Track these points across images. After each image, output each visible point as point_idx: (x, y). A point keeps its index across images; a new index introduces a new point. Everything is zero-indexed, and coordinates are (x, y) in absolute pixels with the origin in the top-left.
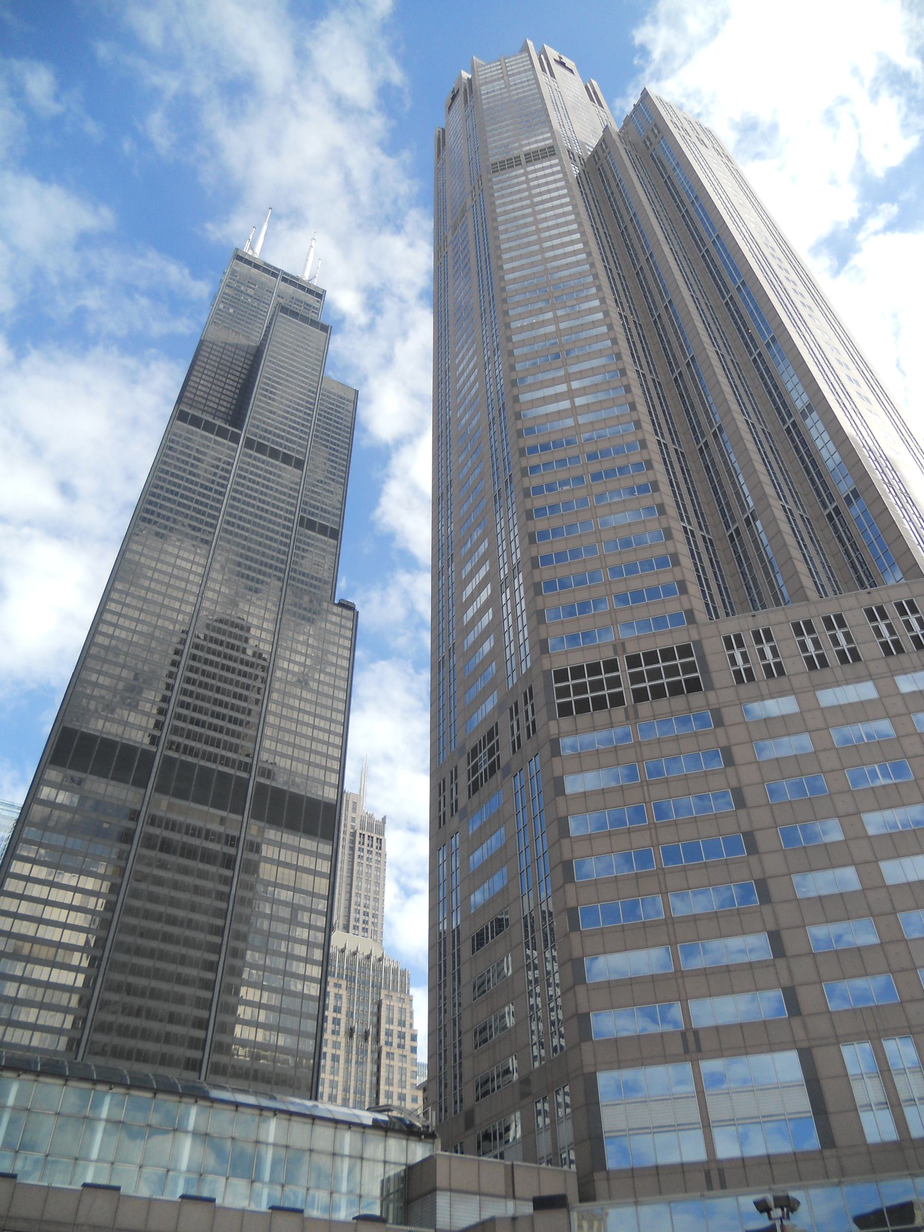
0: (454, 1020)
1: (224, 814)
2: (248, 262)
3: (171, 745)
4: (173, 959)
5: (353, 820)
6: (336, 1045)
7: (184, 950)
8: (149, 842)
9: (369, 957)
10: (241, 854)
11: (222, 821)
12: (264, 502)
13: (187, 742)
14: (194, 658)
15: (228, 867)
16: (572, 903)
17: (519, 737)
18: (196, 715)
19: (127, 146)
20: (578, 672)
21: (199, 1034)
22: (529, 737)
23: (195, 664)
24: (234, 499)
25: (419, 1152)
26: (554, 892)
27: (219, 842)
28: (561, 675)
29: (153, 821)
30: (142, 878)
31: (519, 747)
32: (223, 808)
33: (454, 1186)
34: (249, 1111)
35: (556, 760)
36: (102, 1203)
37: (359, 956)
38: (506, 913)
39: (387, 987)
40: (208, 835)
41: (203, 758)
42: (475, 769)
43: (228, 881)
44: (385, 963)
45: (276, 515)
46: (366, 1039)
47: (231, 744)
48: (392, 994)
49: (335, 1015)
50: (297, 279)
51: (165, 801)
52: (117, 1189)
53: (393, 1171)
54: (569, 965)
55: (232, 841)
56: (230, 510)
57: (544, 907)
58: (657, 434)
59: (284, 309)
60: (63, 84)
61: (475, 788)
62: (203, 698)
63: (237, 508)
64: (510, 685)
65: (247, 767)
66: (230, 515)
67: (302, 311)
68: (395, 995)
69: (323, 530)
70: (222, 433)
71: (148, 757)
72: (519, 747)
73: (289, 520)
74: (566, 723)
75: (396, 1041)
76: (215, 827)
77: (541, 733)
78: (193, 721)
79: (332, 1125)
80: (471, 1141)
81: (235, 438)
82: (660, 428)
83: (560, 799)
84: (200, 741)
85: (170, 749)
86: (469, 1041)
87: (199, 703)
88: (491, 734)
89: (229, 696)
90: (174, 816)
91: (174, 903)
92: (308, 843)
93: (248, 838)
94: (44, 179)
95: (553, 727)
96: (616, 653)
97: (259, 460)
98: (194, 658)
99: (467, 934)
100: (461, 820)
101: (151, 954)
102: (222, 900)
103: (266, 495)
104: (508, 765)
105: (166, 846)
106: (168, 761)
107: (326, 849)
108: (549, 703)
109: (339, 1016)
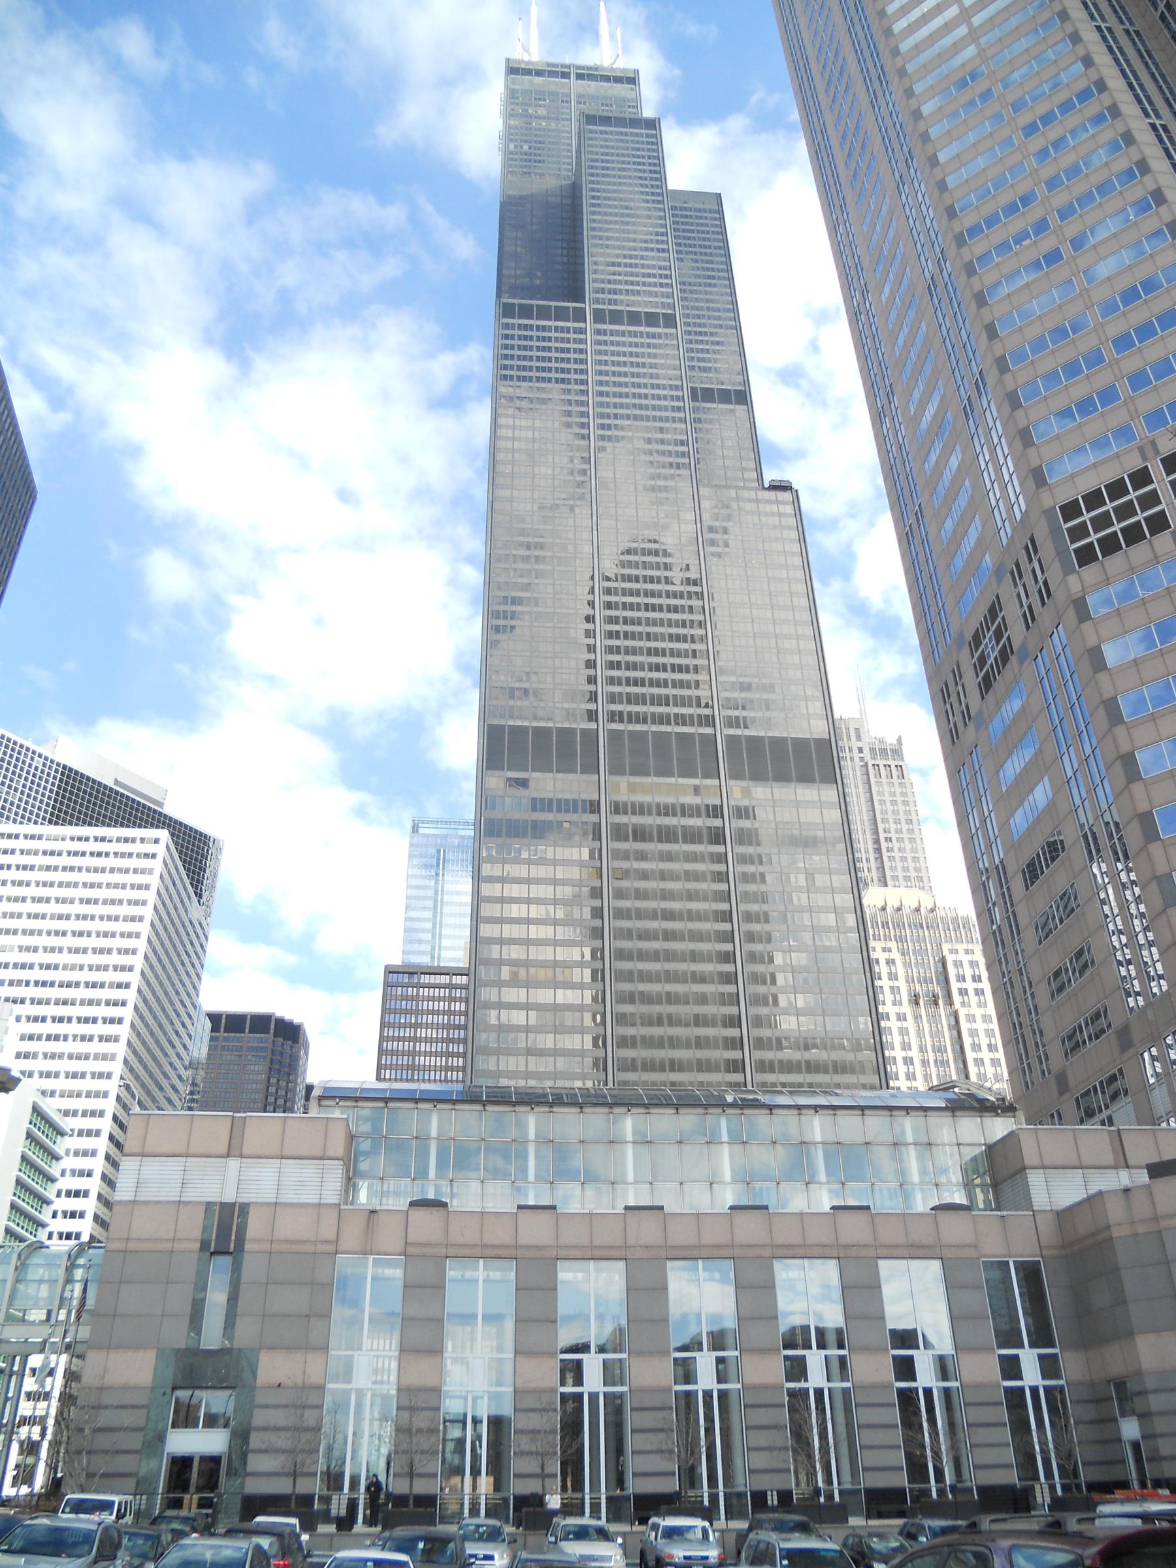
0: (1020, 970)
1: (696, 781)
2: (528, 72)
3: (613, 717)
4: (682, 957)
5: (861, 750)
6: (901, 1017)
7: (692, 946)
8: (619, 833)
9: (918, 910)
10: (731, 825)
11: (696, 790)
12: (639, 386)
13: (630, 708)
14: (609, 606)
15: (718, 843)
16: (1143, 806)
17: (1030, 608)
18: (632, 674)
19: (253, 79)
20: (1094, 499)
21: (733, 1032)
22: (1043, 603)
23: (613, 613)
24: (601, 394)
25: (999, 1127)
26: (1116, 797)
27: (699, 816)
28: (1070, 510)
29: (617, 808)
30: (625, 874)
31: (1033, 619)
32: (693, 775)
33: (1046, 1163)
34: (785, 1112)
35: (1087, 626)
36: (649, 1222)
37: (906, 911)
38: (1059, 833)
40: (686, 811)
41: (653, 723)
42: (982, 660)
43: (722, 858)
44: (940, 913)
45: (659, 397)
46: (936, 1004)
47: (683, 697)
49: (891, 983)
50: (596, 69)
51: (623, 782)
52: (661, 1208)
53: (969, 1153)
54: (1154, 886)
55: (715, 811)
56: (600, 410)
57: (1107, 818)
58: (1147, 115)
59: (591, 119)
60: (159, 34)
61: (987, 685)
62: (634, 651)
63: (608, 405)
64: (1005, 542)
65: (709, 721)
66: (602, 416)
67: (614, 112)
69: (725, 396)
70: (561, 314)
71: (590, 738)
72: (1033, 619)
73: (678, 398)
74: (1090, 573)
76: (690, 799)
77: (1059, 594)
78: (629, 681)
79: (887, 1113)
80: (1069, 1107)
81: (580, 316)
82: (1151, 103)
83: (1102, 677)
84: (644, 703)
85: (613, 721)
86: (1043, 992)
87: (631, 658)
88: (993, 611)
89: (663, 640)
90: (638, 798)
91: (666, 895)
92: (806, 793)
93: (732, 803)
94: (184, 157)
95: (1073, 584)
96: (1145, 459)
97: (617, 333)
98: (609, 606)
99: (1015, 867)
100: (977, 729)
101: (656, 956)
102: (720, 881)
103: (638, 375)
104: (1024, 646)
105: (640, 834)
106: (614, 736)
107: (829, 793)
108: (1062, 553)
109: (896, 983)
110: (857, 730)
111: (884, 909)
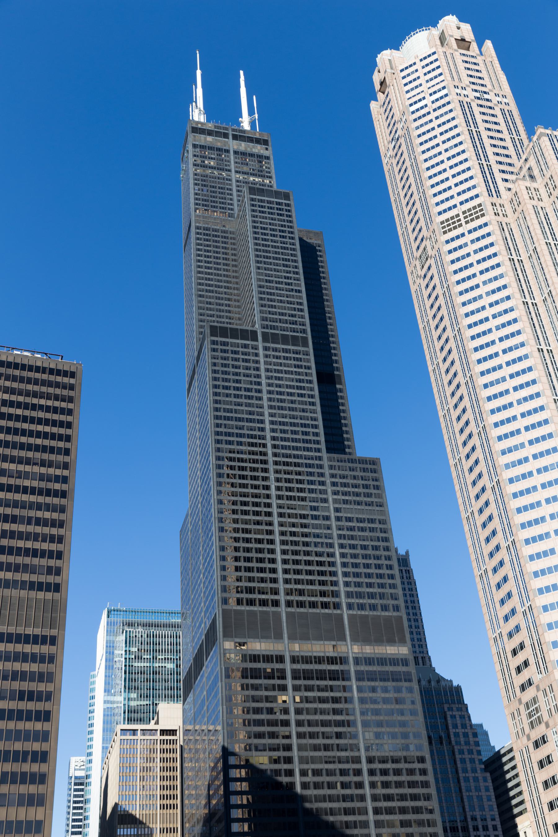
29: (294, 660)
39: (447, 702)
46: (441, 743)
48: (453, 706)
68: (454, 707)
75: (462, 740)
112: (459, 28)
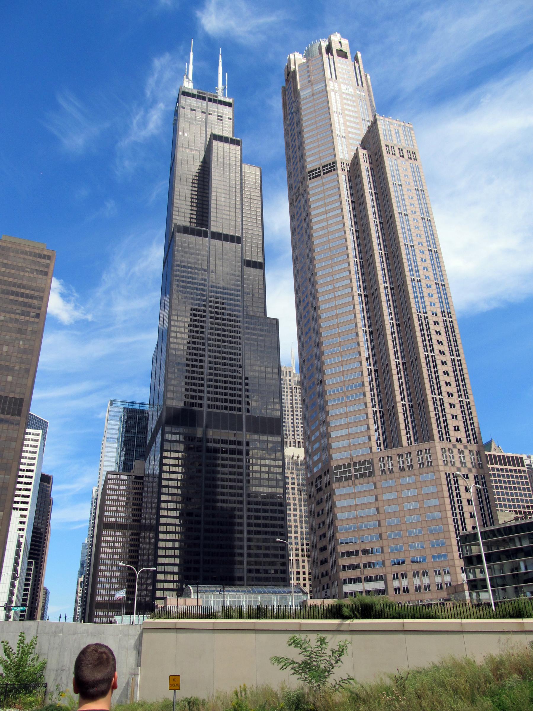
1: (235, 432)
11: (235, 435)
110: (290, 372)
111: (293, 457)
112: (340, 42)
